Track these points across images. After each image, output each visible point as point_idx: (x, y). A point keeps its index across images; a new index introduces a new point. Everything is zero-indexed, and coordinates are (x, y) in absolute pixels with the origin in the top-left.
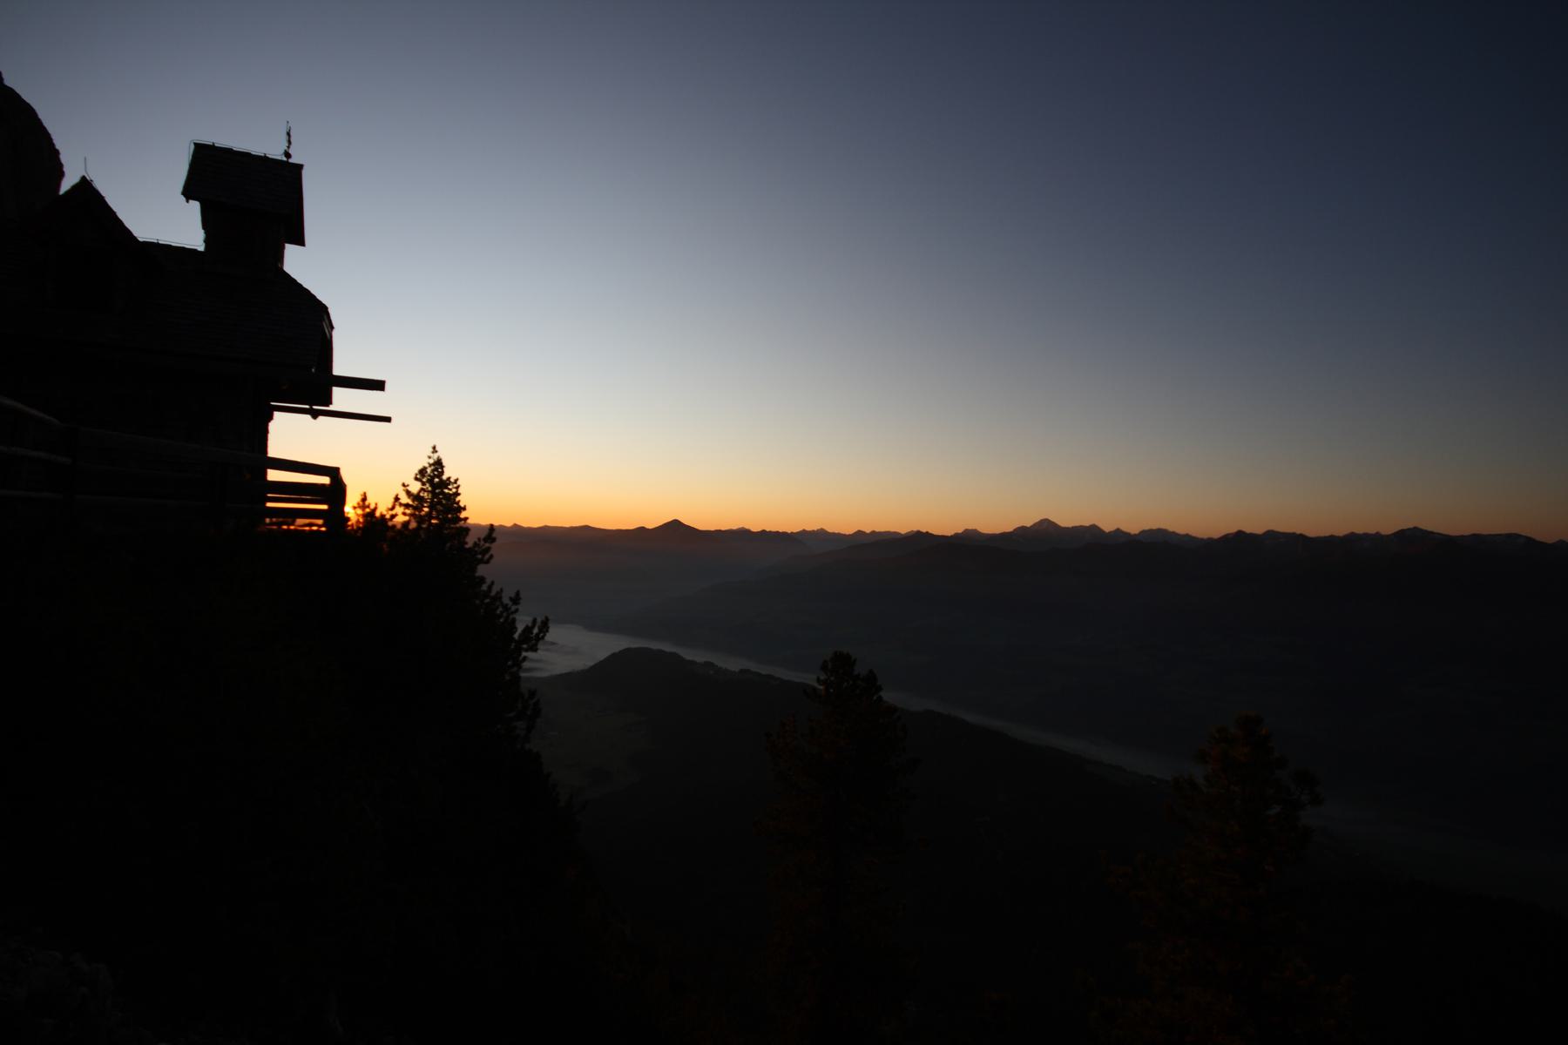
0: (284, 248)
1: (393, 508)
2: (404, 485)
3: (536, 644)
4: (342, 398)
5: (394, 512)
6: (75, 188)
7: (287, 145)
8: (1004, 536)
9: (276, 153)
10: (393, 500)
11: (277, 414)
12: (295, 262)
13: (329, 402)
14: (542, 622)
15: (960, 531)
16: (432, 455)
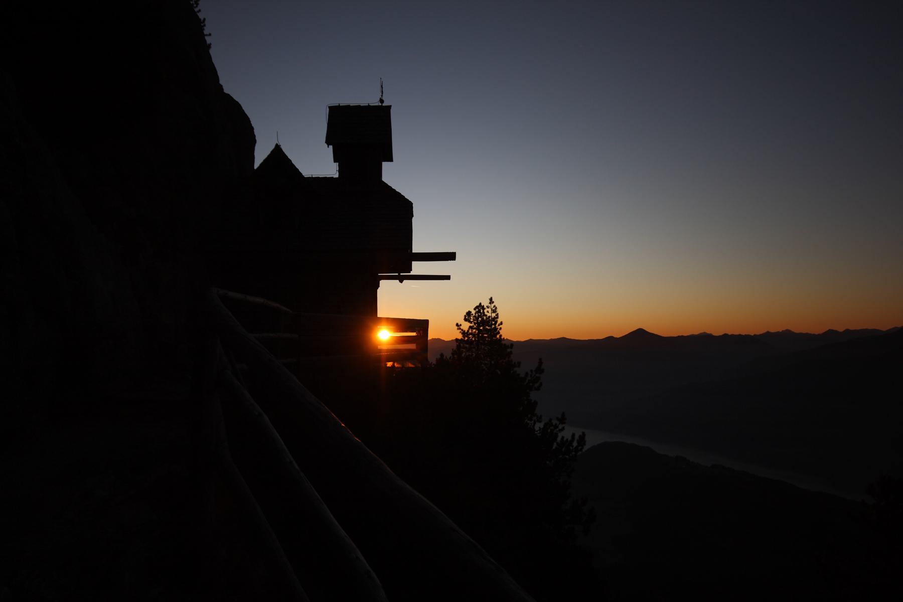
2: (457, 325)
9: (375, 102)
11: (382, 282)
13: (410, 270)
14: (580, 436)
16: (490, 305)
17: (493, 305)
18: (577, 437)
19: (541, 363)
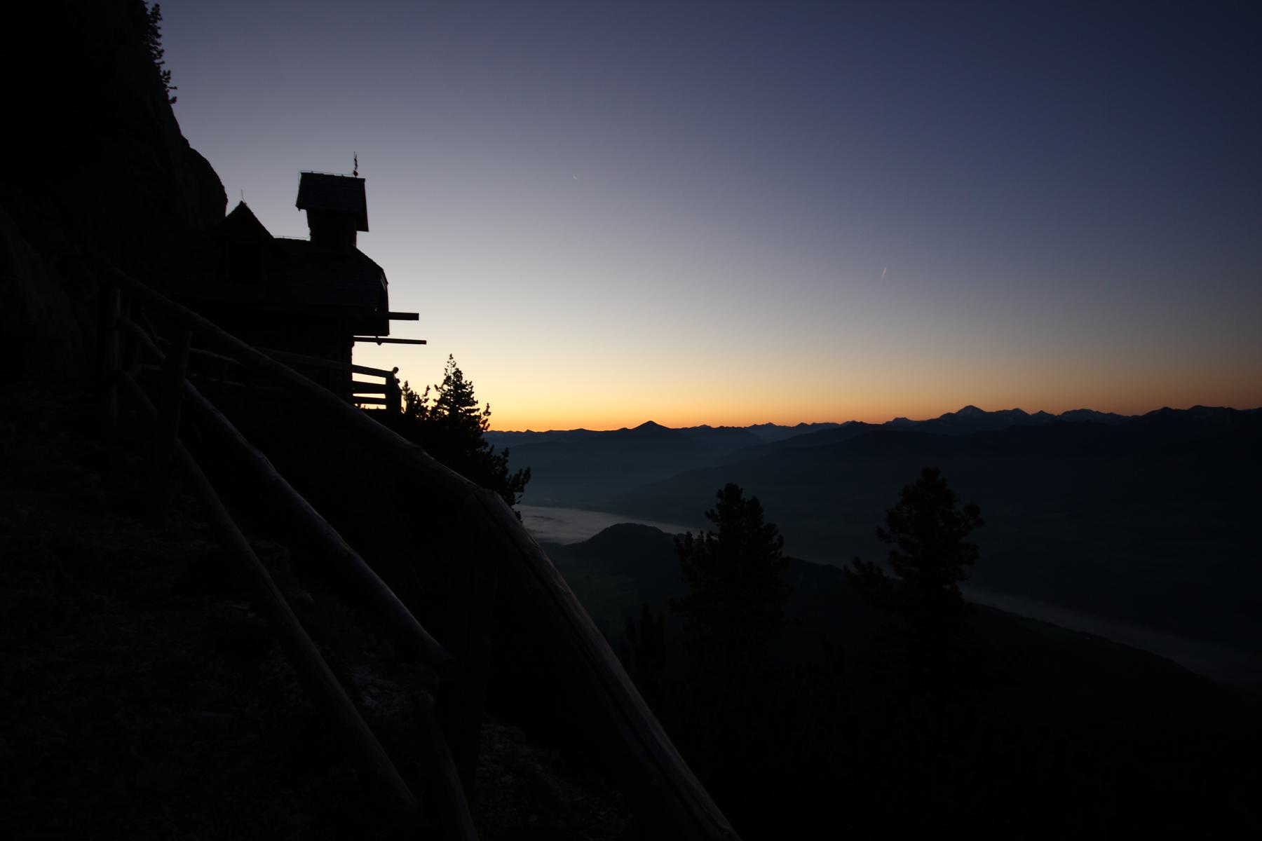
0: (356, 234)
1: (426, 395)
3: (522, 487)
4: (397, 328)
5: (426, 397)
6: (237, 209)
7: (355, 166)
8: (931, 423)
10: (426, 390)
11: (356, 343)
12: (365, 243)
13: (387, 333)
14: (526, 471)
15: (891, 419)
16: (449, 360)
17: (452, 360)
18: (524, 472)
19: (488, 407)
